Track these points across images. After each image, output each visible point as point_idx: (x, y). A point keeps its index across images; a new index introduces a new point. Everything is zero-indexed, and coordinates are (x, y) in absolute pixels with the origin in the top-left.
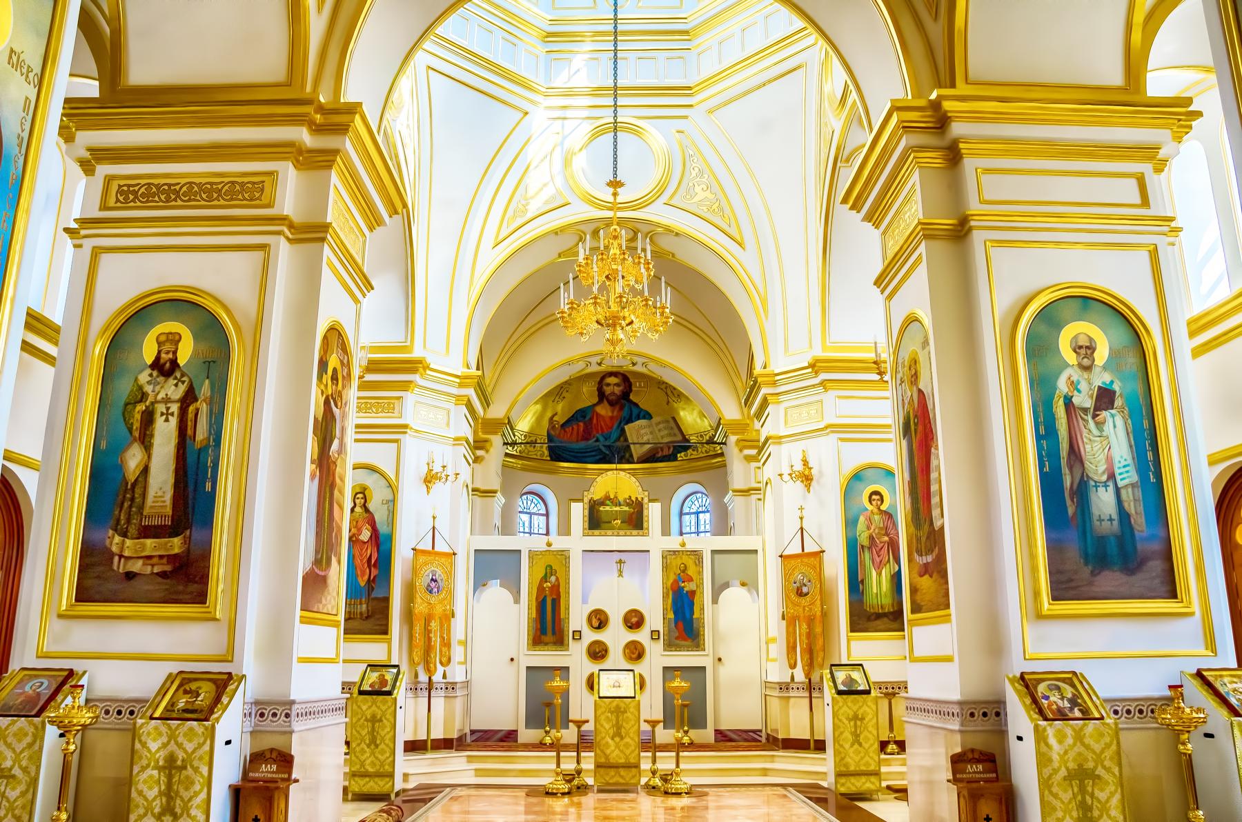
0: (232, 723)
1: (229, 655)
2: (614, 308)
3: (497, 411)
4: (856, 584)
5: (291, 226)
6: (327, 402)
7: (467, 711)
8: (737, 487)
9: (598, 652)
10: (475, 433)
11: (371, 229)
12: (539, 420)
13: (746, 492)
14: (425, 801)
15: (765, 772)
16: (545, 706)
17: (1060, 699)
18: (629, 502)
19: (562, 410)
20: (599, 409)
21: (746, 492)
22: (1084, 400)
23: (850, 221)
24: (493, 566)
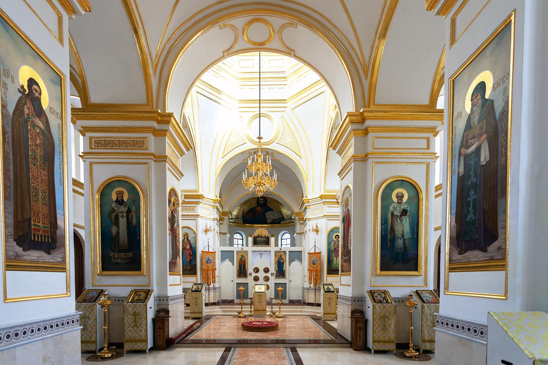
0: (151, 303)
1: (149, 284)
2: (259, 180)
3: (226, 209)
4: (330, 261)
5: (155, 156)
6: (172, 212)
7: (220, 295)
8: (297, 232)
9: (256, 279)
10: (220, 216)
11: (181, 156)
12: (239, 211)
13: (300, 234)
14: (208, 319)
15: (301, 311)
16: (242, 293)
17: (380, 297)
18: (265, 237)
19: (246, 208)
20: (257, 208)
21: (300, 234)
22: (397, 213)
23: (333, 153)
24: (226, 255)
